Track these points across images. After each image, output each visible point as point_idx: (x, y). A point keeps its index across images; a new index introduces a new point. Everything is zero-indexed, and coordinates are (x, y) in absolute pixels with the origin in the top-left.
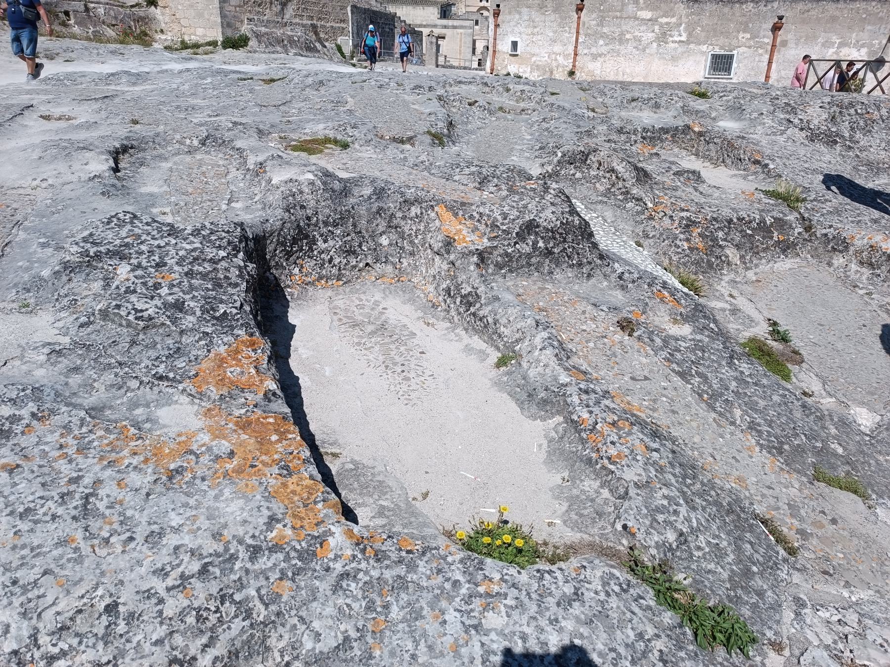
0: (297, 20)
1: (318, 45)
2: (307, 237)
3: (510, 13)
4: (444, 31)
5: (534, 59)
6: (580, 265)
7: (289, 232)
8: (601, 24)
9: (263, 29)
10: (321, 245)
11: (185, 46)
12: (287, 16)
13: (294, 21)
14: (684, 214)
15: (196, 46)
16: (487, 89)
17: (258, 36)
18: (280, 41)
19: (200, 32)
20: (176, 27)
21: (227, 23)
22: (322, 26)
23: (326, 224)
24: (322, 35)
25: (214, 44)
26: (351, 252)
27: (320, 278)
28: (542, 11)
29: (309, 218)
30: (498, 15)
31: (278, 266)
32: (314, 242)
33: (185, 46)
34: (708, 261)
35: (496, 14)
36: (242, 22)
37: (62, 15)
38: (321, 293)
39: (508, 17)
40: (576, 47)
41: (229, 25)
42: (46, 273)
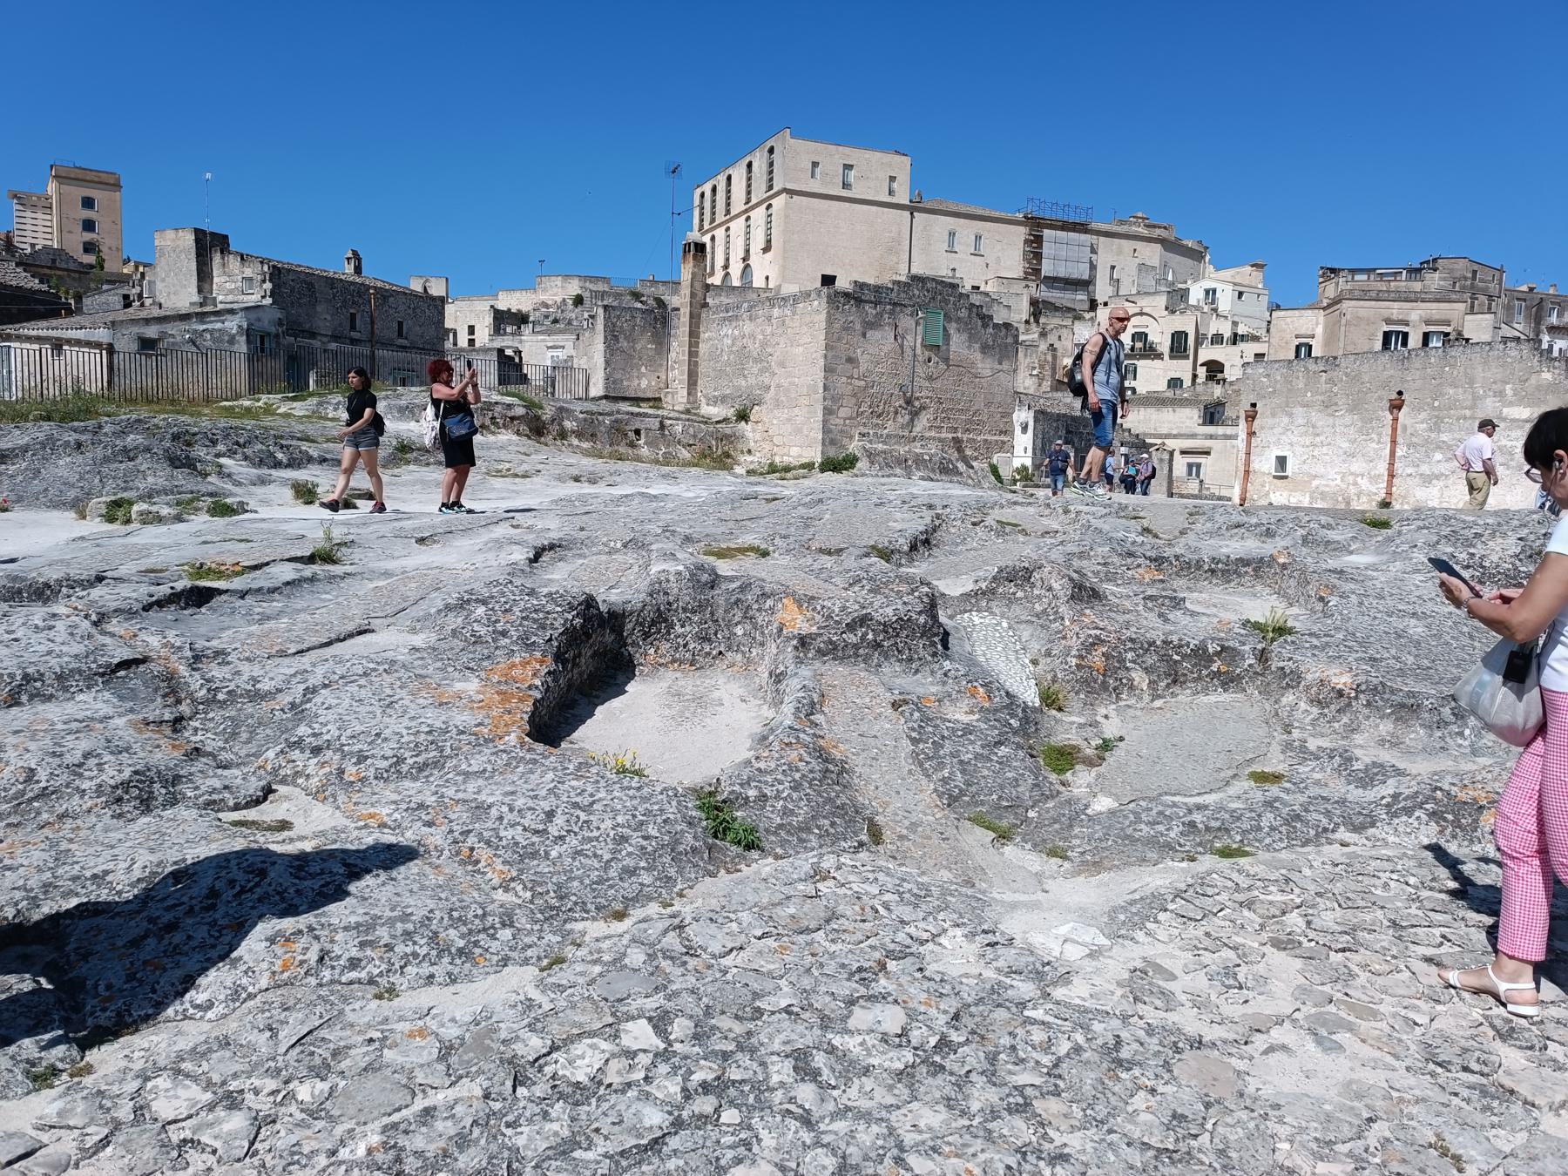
0: (933, 434)
1: (961, 466)
2: (666, 620)
3: (1273, 415)
4: (1208, 443)
5: (1315, 483)
6: (910, 660)
7: (649, 614)
8: (1436, 427)
9: (880, 446)
10: (679, 629)
11: (773, 469)
12: (918, 429)
13: (927, 434)
14: (1093, 632)
15: (787, 469)
16: (1047, 512)
17: (871, 455)
18: (902, 461)
19: (795, 451)
20: (767, 446)
21: (829, 438)
22: (969, 440)
23: (685, 610)
24: (968, 452)
25: (809, 466)
26: (707, 639)
27: (674, 661)
28: (1330, 411)
29: (669, 604)
30: (1254, 418)
31: (634, 644)
32: (672, 626)
33: (773, 469)
34: (1104, 682)
35: (1251, 417)
36: (851, 437)
37: (632, 435)
38: (669, 676)
39: (1270, 421)
40: (1391, 464)
41: (833, 442)
42: (433, 611)
